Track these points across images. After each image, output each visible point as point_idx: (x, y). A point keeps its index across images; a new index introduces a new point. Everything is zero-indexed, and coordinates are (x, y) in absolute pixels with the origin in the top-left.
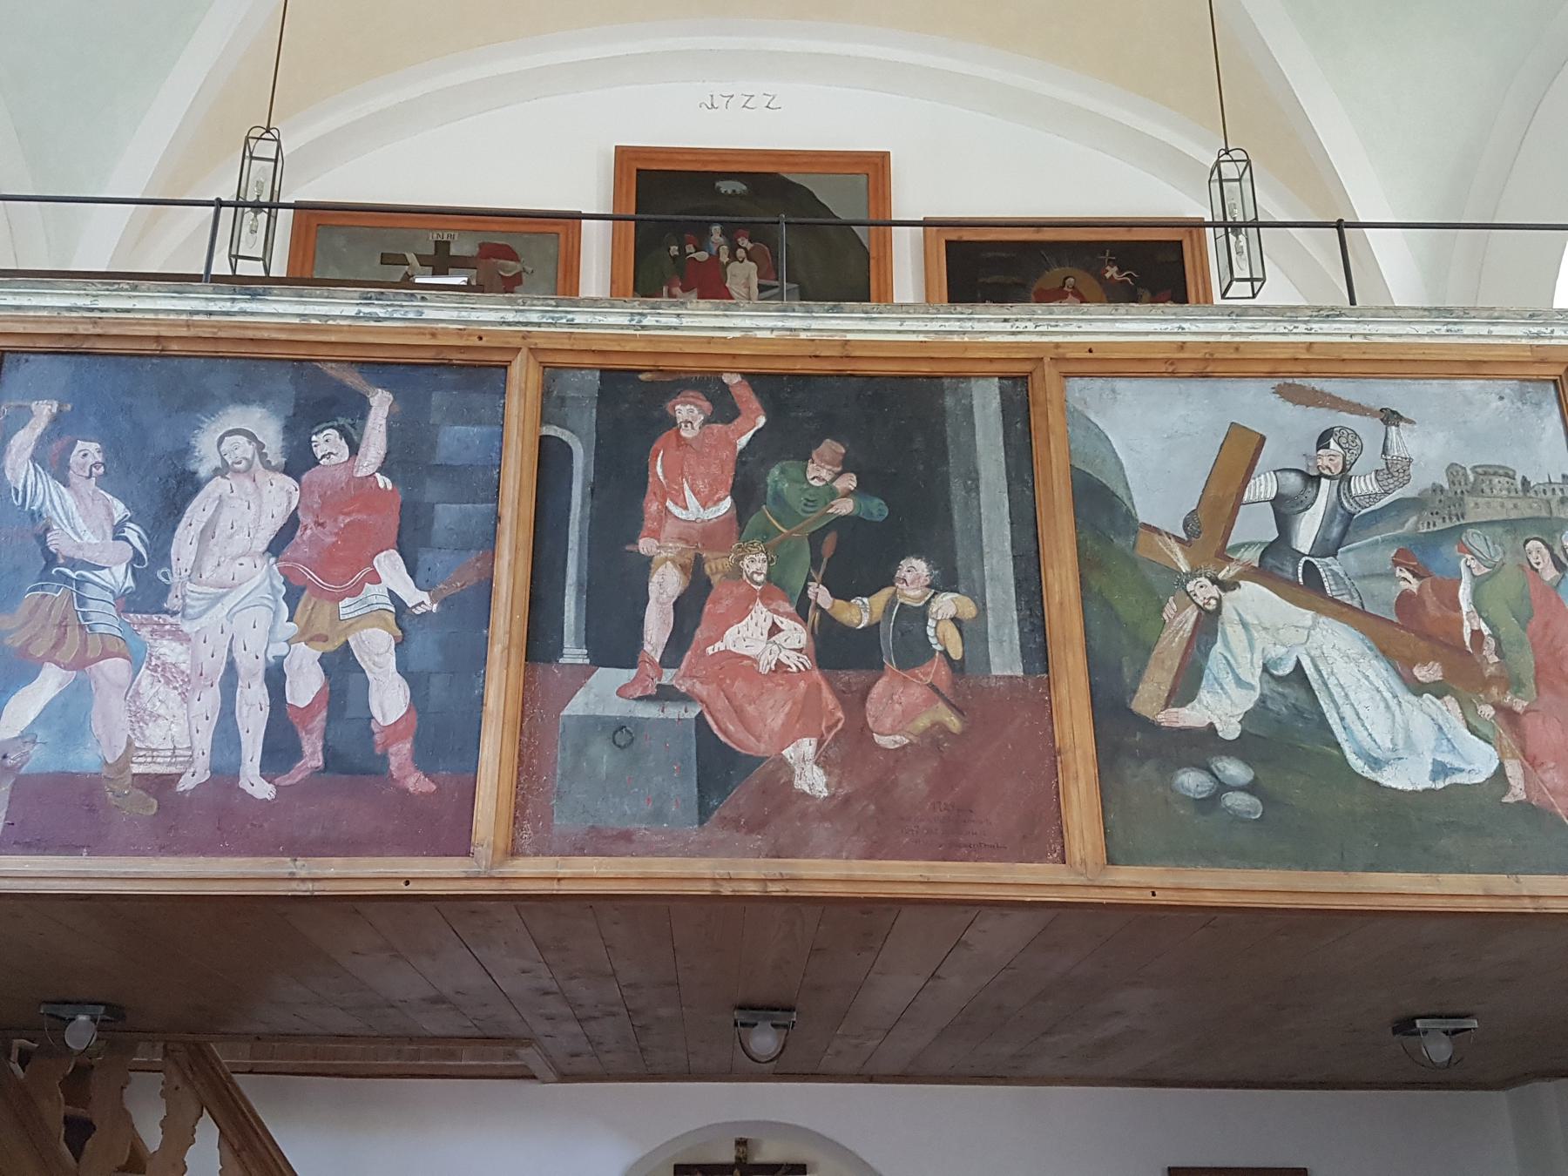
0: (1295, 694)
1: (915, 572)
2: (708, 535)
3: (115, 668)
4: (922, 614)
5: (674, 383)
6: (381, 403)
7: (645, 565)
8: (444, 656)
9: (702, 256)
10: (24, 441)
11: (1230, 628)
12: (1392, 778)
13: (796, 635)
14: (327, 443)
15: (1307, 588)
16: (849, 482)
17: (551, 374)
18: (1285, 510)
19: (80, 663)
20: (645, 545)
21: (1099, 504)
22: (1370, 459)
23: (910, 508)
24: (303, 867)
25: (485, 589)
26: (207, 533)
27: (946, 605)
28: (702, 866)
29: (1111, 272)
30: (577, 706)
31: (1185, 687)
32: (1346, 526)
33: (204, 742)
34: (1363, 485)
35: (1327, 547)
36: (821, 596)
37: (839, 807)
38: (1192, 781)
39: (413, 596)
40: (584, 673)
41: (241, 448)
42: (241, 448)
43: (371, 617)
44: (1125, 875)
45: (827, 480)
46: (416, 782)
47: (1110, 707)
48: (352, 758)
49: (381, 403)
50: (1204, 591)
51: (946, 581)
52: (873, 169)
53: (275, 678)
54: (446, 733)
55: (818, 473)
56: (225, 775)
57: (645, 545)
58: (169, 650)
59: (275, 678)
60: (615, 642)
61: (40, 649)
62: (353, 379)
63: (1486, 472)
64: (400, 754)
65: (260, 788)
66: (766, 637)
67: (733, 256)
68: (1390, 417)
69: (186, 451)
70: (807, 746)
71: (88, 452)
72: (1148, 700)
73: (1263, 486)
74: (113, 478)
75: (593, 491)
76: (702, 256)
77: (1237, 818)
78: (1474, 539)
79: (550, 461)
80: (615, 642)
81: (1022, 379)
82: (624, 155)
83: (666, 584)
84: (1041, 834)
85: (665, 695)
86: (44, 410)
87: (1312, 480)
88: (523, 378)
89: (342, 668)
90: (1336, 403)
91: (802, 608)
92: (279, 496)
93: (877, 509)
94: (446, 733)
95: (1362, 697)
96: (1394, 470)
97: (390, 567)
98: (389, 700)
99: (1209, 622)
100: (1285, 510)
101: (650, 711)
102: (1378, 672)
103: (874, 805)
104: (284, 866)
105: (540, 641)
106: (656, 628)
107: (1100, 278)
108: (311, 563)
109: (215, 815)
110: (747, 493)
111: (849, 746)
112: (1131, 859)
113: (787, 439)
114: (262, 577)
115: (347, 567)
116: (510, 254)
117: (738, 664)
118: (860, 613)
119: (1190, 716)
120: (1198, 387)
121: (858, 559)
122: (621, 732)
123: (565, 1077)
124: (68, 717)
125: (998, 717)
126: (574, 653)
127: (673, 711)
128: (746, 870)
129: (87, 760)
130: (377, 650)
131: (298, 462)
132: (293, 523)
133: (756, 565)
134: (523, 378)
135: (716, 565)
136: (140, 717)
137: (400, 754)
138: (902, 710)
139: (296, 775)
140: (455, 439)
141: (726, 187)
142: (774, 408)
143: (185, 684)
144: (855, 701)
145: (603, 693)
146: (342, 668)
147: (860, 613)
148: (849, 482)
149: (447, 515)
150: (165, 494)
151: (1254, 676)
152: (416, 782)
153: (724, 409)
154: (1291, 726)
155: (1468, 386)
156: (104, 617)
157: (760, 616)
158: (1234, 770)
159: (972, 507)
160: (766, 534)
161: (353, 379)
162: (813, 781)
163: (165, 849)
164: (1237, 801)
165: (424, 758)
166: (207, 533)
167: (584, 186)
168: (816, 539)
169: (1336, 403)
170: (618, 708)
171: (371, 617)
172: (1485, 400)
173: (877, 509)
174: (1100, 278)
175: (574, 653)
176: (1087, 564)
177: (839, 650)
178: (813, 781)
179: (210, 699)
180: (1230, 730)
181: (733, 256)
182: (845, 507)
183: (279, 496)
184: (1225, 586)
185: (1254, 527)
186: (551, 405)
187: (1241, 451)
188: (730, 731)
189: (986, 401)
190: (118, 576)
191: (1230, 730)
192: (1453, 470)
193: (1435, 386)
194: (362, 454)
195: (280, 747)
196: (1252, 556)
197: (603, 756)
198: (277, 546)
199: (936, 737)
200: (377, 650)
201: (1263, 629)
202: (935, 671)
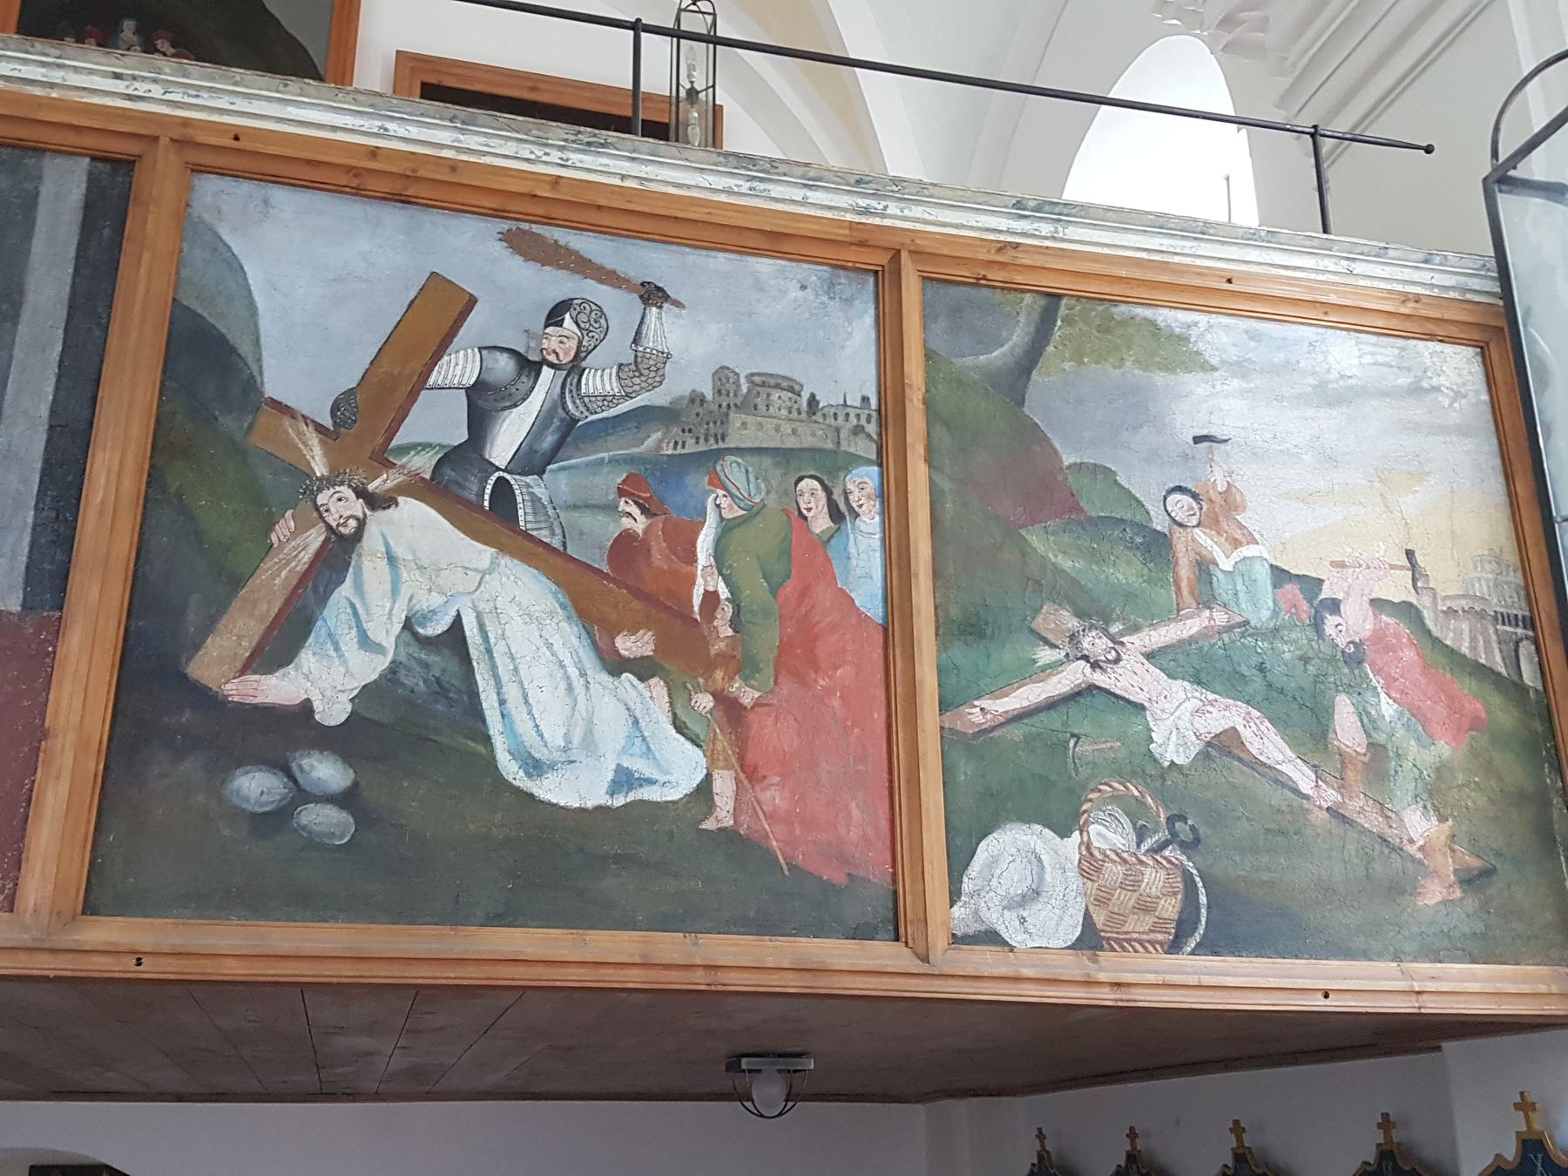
0: (440, 662)
11: (370, 564)
15: (493, 517)
18: (483, 403)
21: (207, 363)
22: (616, 347)
31: (281, 643)
32: (564, 434)
34: (597, 382)
35: (531, 461)
38: (255, 787)
47: (151, 675)
50: (341, 505)
63: (765, 383)
68: (653, 295)
72: (218, 663)
77: (313, 844)
78: (732, 469)
81: (124, 165)
87: (529, 367)
96: (643, 366)
99: (339, 551)
100: (483, 403)
102: (568, 639)
112: (124, 906)
120: (394, 216)
151: (387, 633)
154: (429, 710)
155: (764, 266)
158: (326, 772)
164: (322, 819)
172: (782, 286)
180: (333, 711)
184: (377, 502)
185: (436, 421)
187: (439, 312)
191: (333, 711)
192: (723, 376)
193: (721, 261)
196: (423, 463)
201: (418, 564)
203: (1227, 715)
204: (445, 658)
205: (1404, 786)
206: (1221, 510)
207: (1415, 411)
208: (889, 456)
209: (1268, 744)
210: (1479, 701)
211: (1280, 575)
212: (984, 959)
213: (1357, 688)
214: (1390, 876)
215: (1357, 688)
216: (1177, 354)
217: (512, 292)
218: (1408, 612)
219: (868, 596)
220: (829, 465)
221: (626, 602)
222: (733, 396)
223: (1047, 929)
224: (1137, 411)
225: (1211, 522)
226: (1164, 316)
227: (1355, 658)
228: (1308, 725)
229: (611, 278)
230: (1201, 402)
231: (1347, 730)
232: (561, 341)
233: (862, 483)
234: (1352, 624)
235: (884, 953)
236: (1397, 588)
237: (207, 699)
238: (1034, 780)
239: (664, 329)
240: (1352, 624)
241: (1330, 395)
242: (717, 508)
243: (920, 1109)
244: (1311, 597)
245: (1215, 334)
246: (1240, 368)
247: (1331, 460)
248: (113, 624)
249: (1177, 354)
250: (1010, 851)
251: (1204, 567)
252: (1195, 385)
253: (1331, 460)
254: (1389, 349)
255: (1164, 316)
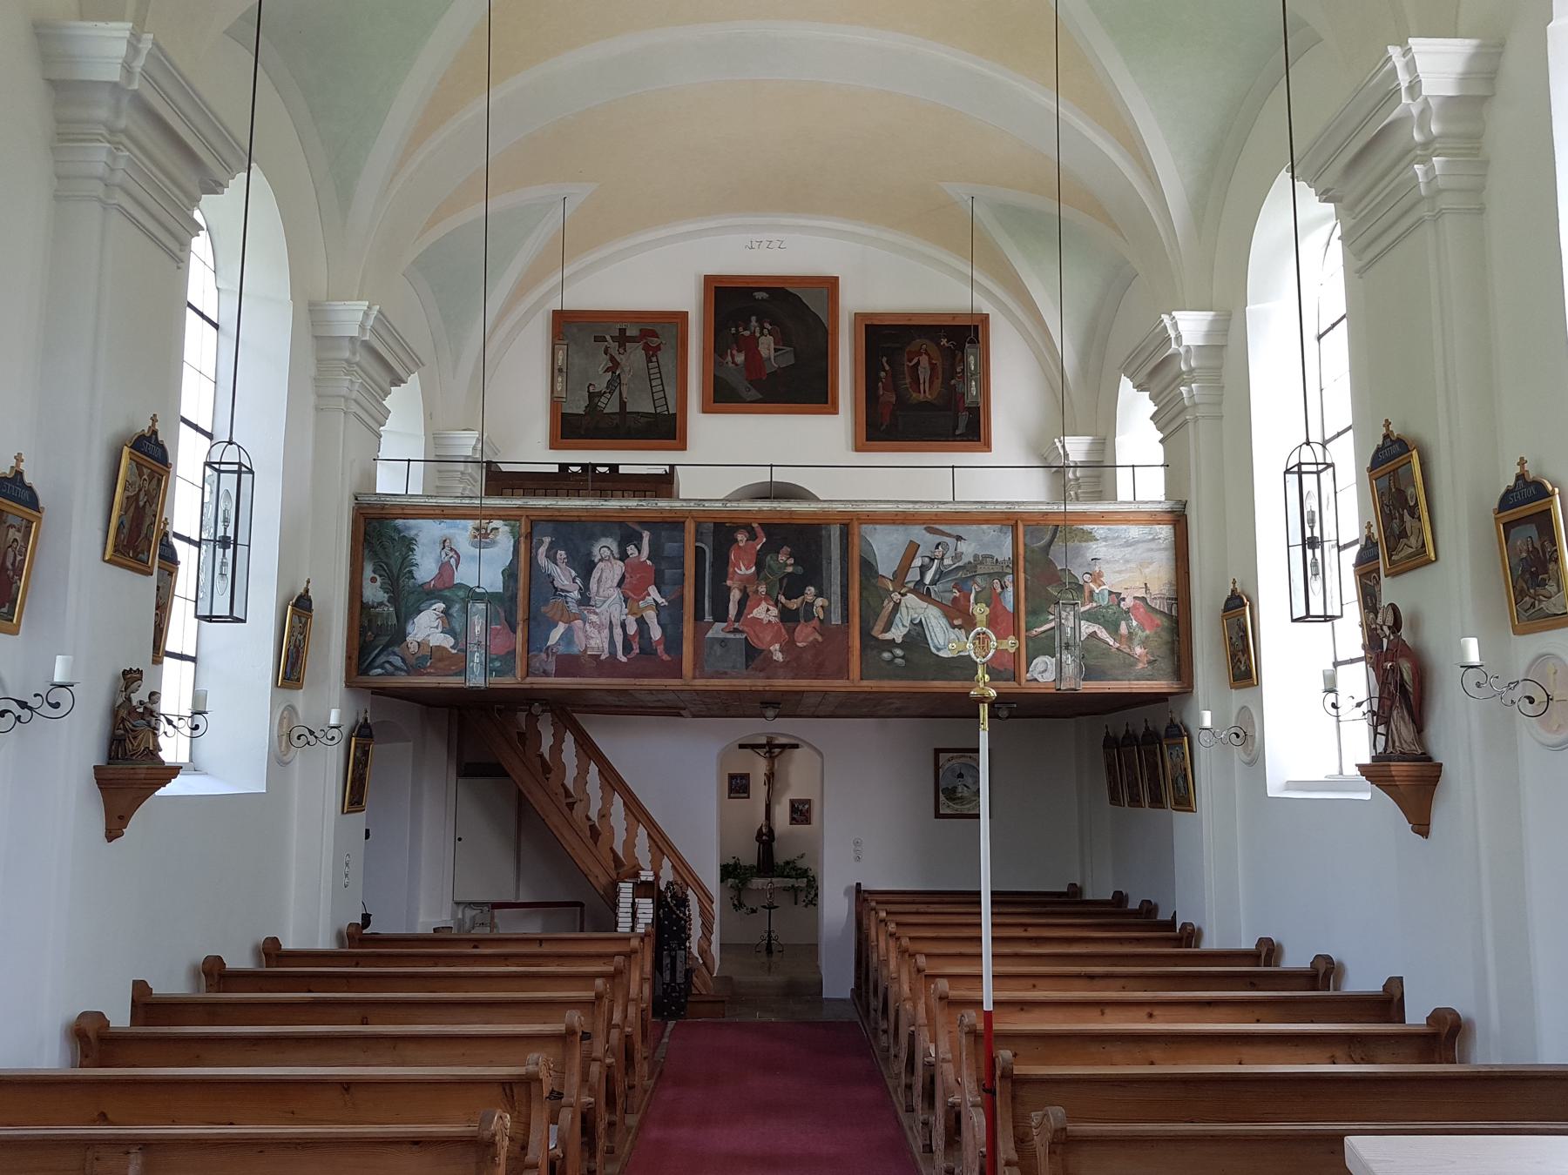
0: (918, 629)
1: (811, 590)
2: (748, 579)
3: (578, 623)
4: (812, 604)
5: (737, 527)
6: (646, 535)
7: (729, 589)
8: (671, 617)
9: (747, 333)
10: (542, 550)
11: (903, 609)
12: (941, 654)
13: (774, 611)
14: (631, 550)
15: (926, 596)
16: (791, 561)
17: (698, 525)
18: (923, 569)
19: (568, 622)
20: (729, 583)
21: (868, 567)
22: (951, 553)
23: (810, 571)
24: (637, 681)
25: (682, 597)
26: (599, 581)
27: (820, 601)
28: (747, 682)
29: (944, 341)
30: (709, 635)
31: (887, 629)
32: (941, 575)
33: (606, 646)
34: (947, 562)
35: (934, 582)
36: (782, 599)
37: (786, 664)
38: (886, 655)
39: (660, 600)
40: (711, 625)
41: (606, 552)
42: (606, 552)
43: (648, 607)
44: (865, 683)
45: (785, 560)
46: (666, 657)
47: (866, 634)
48: (647, 649)
49: (646, 535)
50: (896, 596)
51: (819, 594)
52: (829, 286)
53: (623, 626)
54: (673, 641)
55: (782, 558)
56: (613, 654)
57: (729, 583)
58: (593, 618)
59: (623, 626)
60: (720, 615)
61: (557, 617)
62: (637, 528)
63: (985, 557)
64: (660, 649)
65: (624, 659)
66: (764, 612)
67: (762, 334)
68: (959, 538)
69: (590, 554)
70: (777, 646)
71: (561, 554)
72: (876, 632)
73: (917, 562)
74: (571, 562)
75: (712, 565)
76: (747, 333)
77: (898, 666)
78: (978, 579)
79: (699, 553)
80: (720, 615)
81: (847, 525)
82: (708, 279)
83: (735, 595)
84: (843, 672)
85: (736, 631)
86: (547, 540)
87: (932, 560)
88: (690, 527)
89: (641, 622)
90: (943, 533)
91: (776, 603)
92: (619, 568)
93: (800, 570)
94: (673, 641)
95: (937, 630)
96: (957, 556)
97: (653, 590)
98: (656, 633)
99: (897, 606)
100: (923, 569)
101: (731, 636)
102: (943, 622)
103: (796, 664)
104: (632, 681)
105: (699, 615)
106: (733, 610)
107: (938, 344)
108: (630, 589)
109: (606, 666)
110: (760, 565)
111: (789, 646)
112: (868, 679)
113: (772, 547)
114: (616, 594)
115: (641, 592)
116: (654, 334)
117: (758, 621)
118: (794, 604)
119: (888, 636)
120: (901, 528)
121: (793, 587)
122: (723, 642)
123: (694, 716)
124: (568, 637)
125: (833, 637)
126: (708, 618)
127: (738, 636)
128: (760, 683)
129: (575, 650)
130: (651, 617)
131: (623, 557)
132: (623, 577)
133: (762, 589)
134: (690, 527)
135: (750, 589)
136: (588, 637)
137: (660, 649)
138: (805, 635)
139: (632, 655)
140: (670, 548)
141: (759, 295)
142: (768, 536)
143: (599, 628)
144: (791, 632)
145: (717, 630)
146: (641, 622)
147: (794, 604)
148: (791, 561)
149: (668, 573)
150: (585, 568)
151: (907, 623)
152: (666, 657)
153: (753, 536)
154: (917, 637)
155: (985, 527)
156: (574, 608)
157: (764, 605)
158: (899, 652)
159: (829, 569)
160: (766, 578)
161: (637, 528)
162: (779, 657)
163: (600, 676)
164: (898, 661)
165: (667, 650)
166: (599, 581)
167: (685, 298)
168: (781, 580)
169: (943, 533)
170: (722, 635)
171: (648, 607)
172: (989, 531)
173: (800, 570)
174: (938, 344)
175: (708, 618)
176: (862, 588)
177: (787, 616)
178: (779, 657)
179: (607, 631)
180: (899, 640)
181: (762, 334)
182: (790, 569)
183: (619, 568)
184: (903, 595)
185: (914, 575)
186: (699, 535)
187: (913, 548)
188: (754, 642)
189: (835, 532)
190: (576, 594)
191: (899, 640)
192: (976, 556)
193: (974, 527)
194: (641, 553)
195: (627, 647)
196: (911, 585)
197: (718, 650)
198: (619, 585)
199: (814, 643)
200: (651, 617)
201: (913, 608)
202: (815, 623)
203: (1095, 628)
204: (919, 628)
205: (1136, 641)
206: (1097, 578)
207: (1153, 545)
208: (1015, 572)
209: (1103, 634)
210: (1159, 620)
211: (1111, 593)
212: (1033, 684)
213: (1128, 619)
214: (1131, 661)
215: (1425, 160)
216: (1089, 537)
217: (926, 540)
218: (1143, 599)
219: (1010, 607)
220: (1001, 576)
221: (958, 615)
222: (979, 560)
223: (1049, 677)
224: (1078, 553)
225: (1094, 581)
226: (1087, 527)
227: (1127, 612)
228: (1113, 628)
229: (949, 535)
230: (1097, 549)
231: (1123, 629)
232: (939, 553)
233: (1009, 579)
234: (1128, 603)
235: (1012, 684)
236: (1141, 593)
237: (877, 639)
238: (1044, 646)
239: (962, 547)
240: (1128, 603)
241: (1128, 544)
242: (975, 588)
243: (1072, 720)
244: (1118, 597)
245: (1099, 530)
246: (1105, 539)
247: (1127, 561)
248: (1203, 785)
249: (1089, 537)
250: (1041, 662)
251: (1092, 592)
252: (1093, 545)
253: (1127, 561)
254: (1146, 529)
255: (1087, 527)
